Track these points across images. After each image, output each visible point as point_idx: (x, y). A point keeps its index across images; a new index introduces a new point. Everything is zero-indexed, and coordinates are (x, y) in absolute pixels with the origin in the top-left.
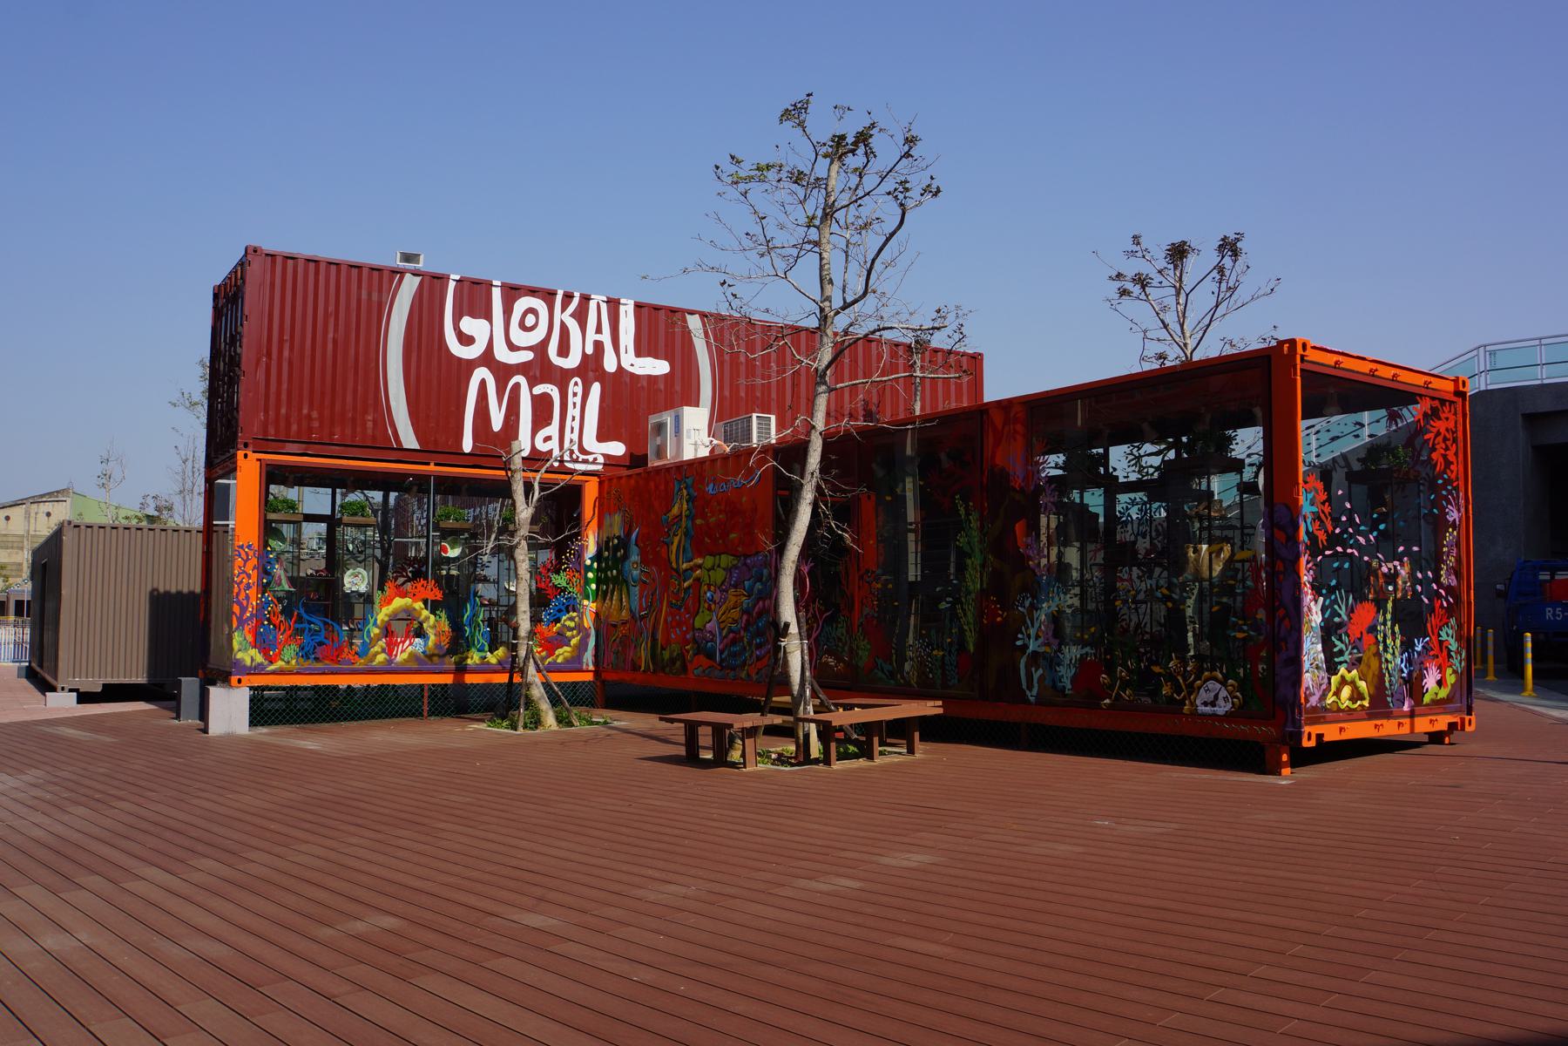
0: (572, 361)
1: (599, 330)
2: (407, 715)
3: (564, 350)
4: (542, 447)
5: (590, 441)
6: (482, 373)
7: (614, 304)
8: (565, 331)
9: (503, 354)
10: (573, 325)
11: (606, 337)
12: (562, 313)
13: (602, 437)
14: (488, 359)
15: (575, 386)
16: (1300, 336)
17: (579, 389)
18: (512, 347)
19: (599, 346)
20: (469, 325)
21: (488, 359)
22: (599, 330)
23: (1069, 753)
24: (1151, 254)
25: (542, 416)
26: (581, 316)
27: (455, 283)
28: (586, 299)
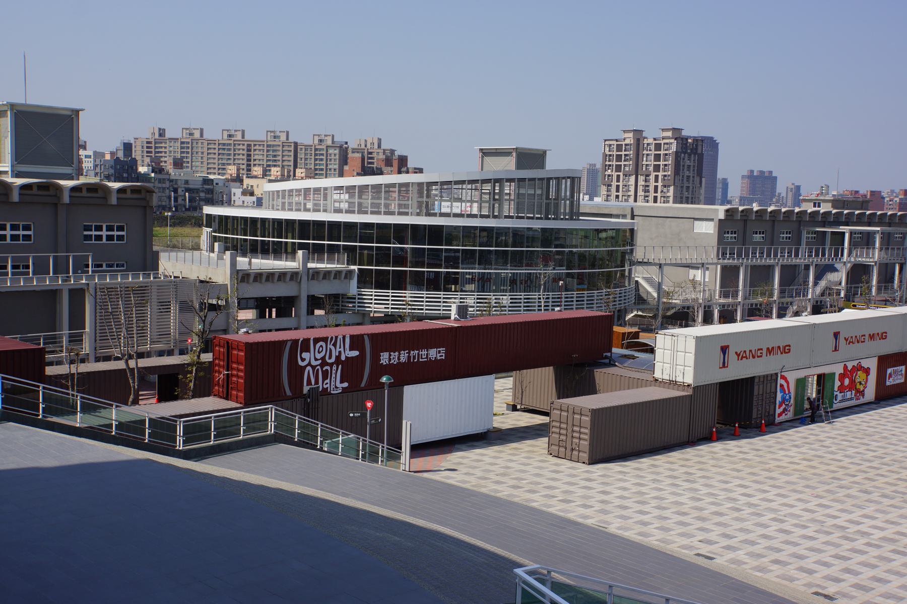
0: (333, 360)
1: (340, 348)
2: (269, 443)
3: (330, 358)
4: (325, 386)
5: (338, 385)
6: (309, 368)
7: (344, 337)
8: (330, 349)
9: (314, 363)
10: (333, 348)
11: (342, 349)
12: (852, 558)
13: (342, 382)
14: (309, 364)
15: (334, 368)
16: (361, 465)
17: (335, 368)
18: (316, 360)
19: (340, 352)
20: (305, 355)
21: (309, 364)
22: (340, 348)
23: (570, 319)
24: (550, 310)
25: (325, 377)
26: (335, 345)
27: (496, 410)
28: (336, 337)
